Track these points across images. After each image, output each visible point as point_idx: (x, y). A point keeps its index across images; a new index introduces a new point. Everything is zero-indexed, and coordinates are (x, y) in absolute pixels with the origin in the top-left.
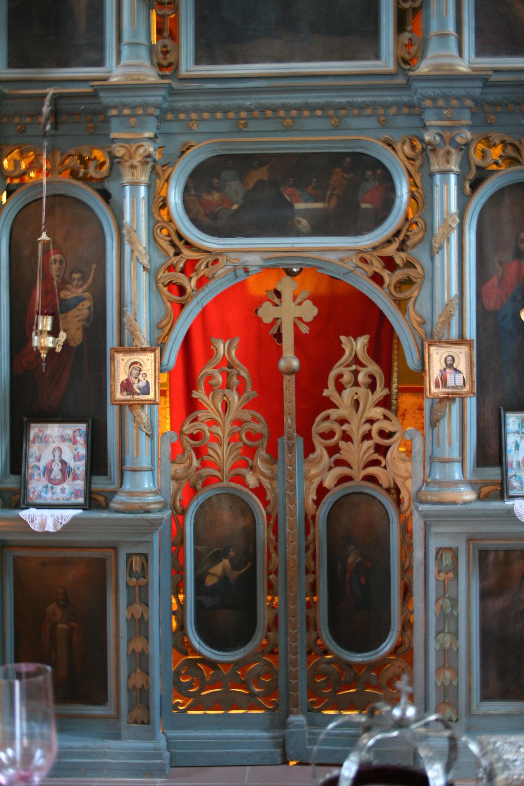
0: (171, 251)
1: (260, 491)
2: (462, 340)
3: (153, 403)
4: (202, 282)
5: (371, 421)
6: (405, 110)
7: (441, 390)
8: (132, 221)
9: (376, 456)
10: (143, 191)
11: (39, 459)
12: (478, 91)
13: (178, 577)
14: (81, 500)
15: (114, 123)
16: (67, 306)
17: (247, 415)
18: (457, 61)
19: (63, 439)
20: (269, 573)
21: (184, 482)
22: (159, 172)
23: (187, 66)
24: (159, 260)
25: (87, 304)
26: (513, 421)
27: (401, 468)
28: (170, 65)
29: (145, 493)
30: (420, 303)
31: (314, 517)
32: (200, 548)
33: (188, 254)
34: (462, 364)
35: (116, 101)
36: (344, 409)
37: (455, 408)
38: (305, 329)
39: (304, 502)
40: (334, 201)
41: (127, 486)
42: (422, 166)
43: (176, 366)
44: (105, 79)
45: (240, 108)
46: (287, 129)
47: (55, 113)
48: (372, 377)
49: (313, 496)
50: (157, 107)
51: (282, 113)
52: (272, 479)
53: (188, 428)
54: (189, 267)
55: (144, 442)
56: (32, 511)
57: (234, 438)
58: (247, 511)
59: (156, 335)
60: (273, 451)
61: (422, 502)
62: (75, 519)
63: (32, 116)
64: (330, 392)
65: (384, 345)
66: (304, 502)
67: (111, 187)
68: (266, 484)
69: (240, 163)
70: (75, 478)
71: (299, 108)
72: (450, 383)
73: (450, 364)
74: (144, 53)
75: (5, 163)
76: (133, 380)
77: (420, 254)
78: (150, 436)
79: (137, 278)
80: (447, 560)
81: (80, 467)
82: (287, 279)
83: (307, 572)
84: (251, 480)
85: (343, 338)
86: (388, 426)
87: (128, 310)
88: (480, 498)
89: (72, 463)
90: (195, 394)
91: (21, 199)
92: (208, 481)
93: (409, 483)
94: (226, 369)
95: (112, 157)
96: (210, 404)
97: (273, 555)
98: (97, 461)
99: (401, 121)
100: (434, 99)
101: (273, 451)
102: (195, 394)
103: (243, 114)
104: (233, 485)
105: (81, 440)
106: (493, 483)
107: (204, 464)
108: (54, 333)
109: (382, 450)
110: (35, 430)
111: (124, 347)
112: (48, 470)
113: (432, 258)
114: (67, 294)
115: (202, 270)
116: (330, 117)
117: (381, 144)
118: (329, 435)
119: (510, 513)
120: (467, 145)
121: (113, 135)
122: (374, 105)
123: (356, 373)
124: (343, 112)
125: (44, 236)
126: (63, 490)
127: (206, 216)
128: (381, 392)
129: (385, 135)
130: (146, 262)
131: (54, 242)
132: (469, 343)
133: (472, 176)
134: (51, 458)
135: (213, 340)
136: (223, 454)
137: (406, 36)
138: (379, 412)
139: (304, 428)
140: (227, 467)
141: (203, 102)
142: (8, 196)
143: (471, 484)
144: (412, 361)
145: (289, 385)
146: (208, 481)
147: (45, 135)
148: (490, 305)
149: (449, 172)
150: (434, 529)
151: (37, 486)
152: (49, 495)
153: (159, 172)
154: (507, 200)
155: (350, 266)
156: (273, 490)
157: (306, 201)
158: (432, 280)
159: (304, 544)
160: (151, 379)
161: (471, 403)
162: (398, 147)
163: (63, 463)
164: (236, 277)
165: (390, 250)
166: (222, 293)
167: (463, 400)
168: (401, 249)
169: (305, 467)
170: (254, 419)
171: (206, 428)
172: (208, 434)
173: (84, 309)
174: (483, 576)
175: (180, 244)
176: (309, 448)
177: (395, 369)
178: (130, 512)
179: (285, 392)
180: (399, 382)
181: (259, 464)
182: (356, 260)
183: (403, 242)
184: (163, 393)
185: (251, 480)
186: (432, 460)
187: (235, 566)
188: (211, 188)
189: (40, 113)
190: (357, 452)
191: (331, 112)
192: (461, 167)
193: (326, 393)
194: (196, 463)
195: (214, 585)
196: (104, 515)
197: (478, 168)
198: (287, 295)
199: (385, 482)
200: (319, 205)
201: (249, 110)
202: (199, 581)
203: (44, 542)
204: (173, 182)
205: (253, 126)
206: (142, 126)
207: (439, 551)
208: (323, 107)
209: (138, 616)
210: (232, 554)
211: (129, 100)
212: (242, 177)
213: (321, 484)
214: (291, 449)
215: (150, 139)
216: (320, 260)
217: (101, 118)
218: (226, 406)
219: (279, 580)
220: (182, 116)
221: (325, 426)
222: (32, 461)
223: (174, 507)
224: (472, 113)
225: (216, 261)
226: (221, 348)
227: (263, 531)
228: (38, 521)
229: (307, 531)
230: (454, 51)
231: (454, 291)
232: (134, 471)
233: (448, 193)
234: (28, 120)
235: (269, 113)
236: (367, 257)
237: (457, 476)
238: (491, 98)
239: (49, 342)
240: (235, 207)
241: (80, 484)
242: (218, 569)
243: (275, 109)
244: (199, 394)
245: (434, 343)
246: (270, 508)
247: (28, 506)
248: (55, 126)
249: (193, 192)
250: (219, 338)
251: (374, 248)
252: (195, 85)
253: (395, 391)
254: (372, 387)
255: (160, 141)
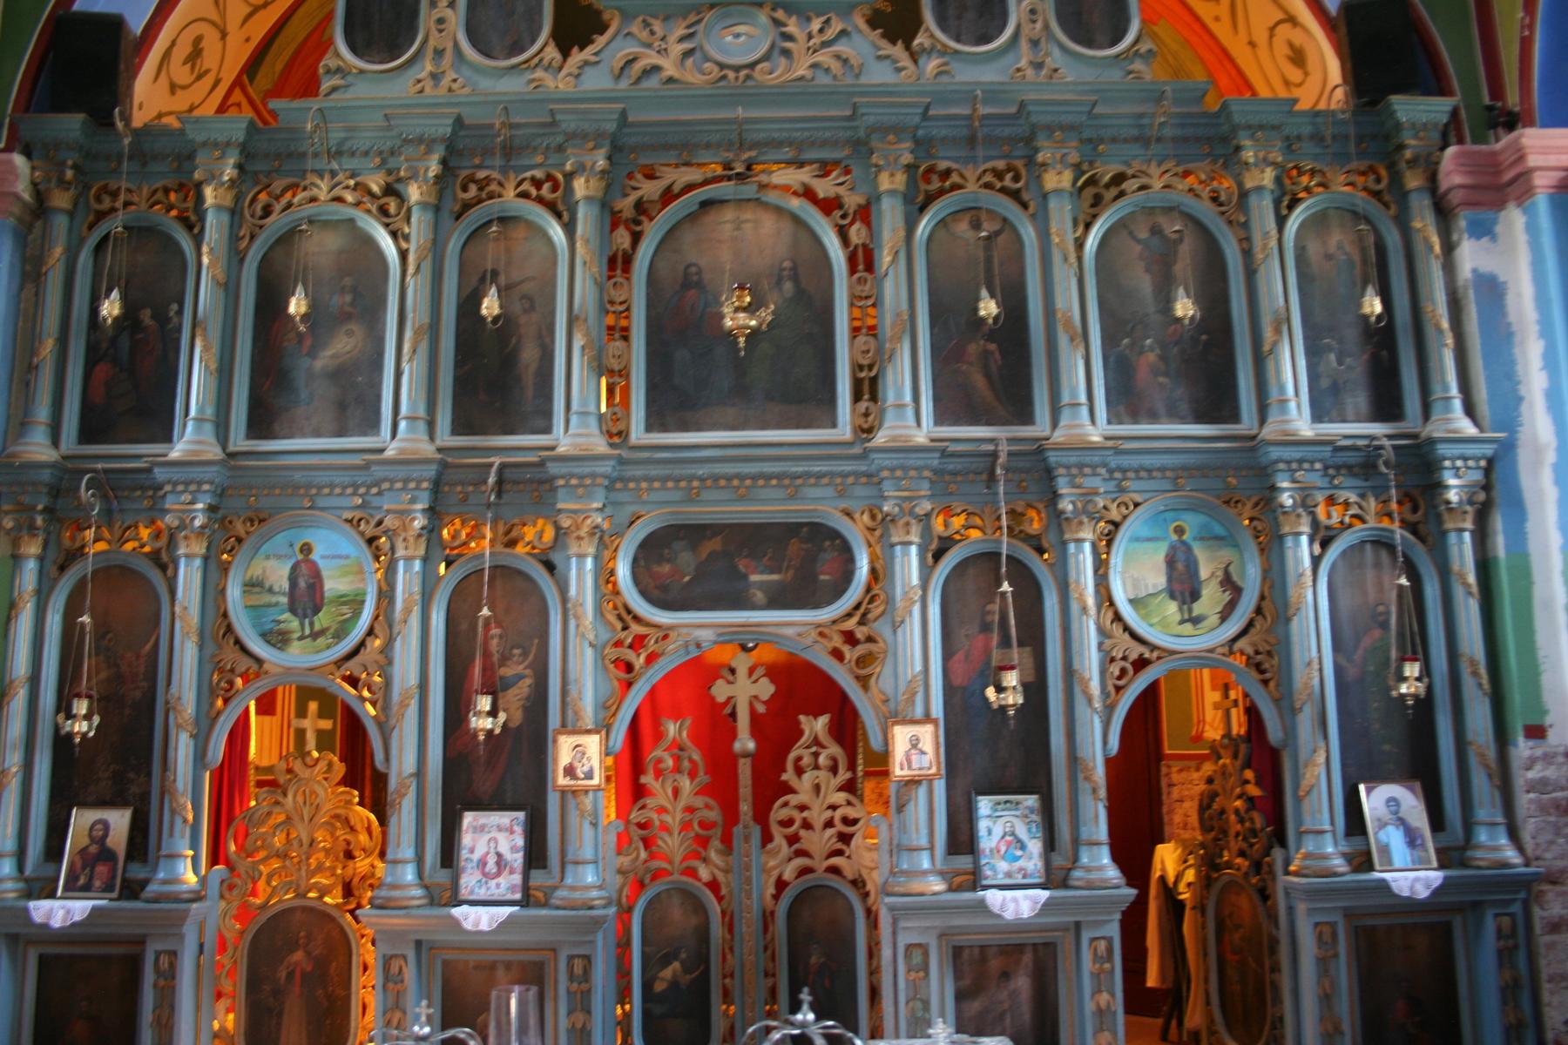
0: (619, 626)
1: (714, 885)
2: (927, 719)
3: (597, 789)
4: (651, 659)
5: (833, 807)
6: (864, 480)
7: (906, 772)
8: (578, 593)
9: (839, 846)
10: (589, 563)
11: (472, 851)
12: (936, 462)
13: (624, 982)
14: (518, 896)
15: (561, 493)
16: (507, 684)
17: (699, 802)
18: (914, 432)
19: (500, 829)
20: (724, 977)
21: (631, 876)
22: (605, 542)
23: (638, 432)
24: (605, 635)
25: (528, 681)
26: (984, 804)
27: (867, 856)
28: (619, 434)
29: (588, 888)
30: (884, 680)
31: (772, 913)
32: (647, 949)
33: (637, 629)
34: (927, 744)
35: (564, 471)
36: (803, 797)
37: (922, 792)
38: (761, 709)
39: (761, 897)
40: (791, 573)
41: (569, 881)
42: (882, 536)
43: (623, 750)
44: (553, 448)
45: (692, 478)
46: (742, 499)
47: (500, 482)
48: (834, 760)
49: (771, 890)
50: (606, 477)
51: (736, 482)
52: (726, 871)
53: (635, 816)
54: (638, 643)
55: (588, 832)
56: (465, 908)
57: (686, 826)
58: (699, 908)
59: (601, 716)
60: (727, 840)
61: (888, 895)
62: (511, 916)
63: (475, 485)
64: (788, 776)
65: (846, 727)
66: (761, 897)
67: (556, 558)
68: (721, 877)
69: (693, 533)
70: (512, 872)
71: (754, 478)
72: (915, 766)
73: (915, 743)
74: (593, 422)
75: (445, 532)
76: (576, 764)
77: (882, 628)
78: (594, 825)
79: (582, 654)
80: (917, 958)
81: (517, 859)
82: (742, 656)
83: (766, 975)
84: (704, 873)
85: (802, 718)
86: (852, 813)
87: (573, 689)
88: (951, 889)
89: (508, 856)
90: (644, 780)
91: (459, 571)
92: (657, 875)
93: (875, 874)
94: (676, 751)
95: (558, 528)
96: (659, 790)
97: (729, 956)
98: (535, 855)
99: (860, 491)
100: (892, 470)
101: (727, 840)
102: (644, 780)
103: (695, 484)
104: (685, 878)
105: (519, 829)
106: (966, 873)
107: (652, 856)
108: (493, 713)
109: (845, 838)
110: (469, 818)
111: (567, 728)
112: (482, 863)
113: (895, 632)
114: (507, 672)
115: (651, 646)
116: (787, 487)
117: (839, 515)
118: (788, 823)
119: (982, 906)
120: (928, 515)
121: (560, 506)
122: (832, 475)
123: (816, 755)
124: (799, 481)
125: (485, 611)
126: (498, 886)
127: (657, 587)
128: (843, 775)
129: (843, 505)
130: (591, 637)
131: (495, 616)
132: (935, 722)
133: (934, 546)
134: (485, 850)
135: (664, 720)
136: (673, 844)
137: (863, 405)
138: (841, 797)
139: (761, 816)
140: (678, 858)
141: (654, 471)
142: (447, 567)
143: (941, 873)
144: (876, 743)
145: (745, 769)
146: (657, 875)
147: (489, 505)
148: (957, 681)
149: (910, 543)
150: (902, 924)
151: (470, 882)
152: (483, 891)
153: (605, 542)
154: (971, 571)
155: (809, 641)
156: (728, 885)
157: (762, 573)
158: (895, 654)
159: (762, 944)
160: (596, 763)
161: (940, 787)
162: (857, 516)
163: (499, 855)
164: (688, 653)
165: (851, 624)
166: (674, 671)
167: (931, 781)
168: (861, 623)
169: (763, 858)
170: (707, 807)
171: (655, 816)
172: (657, 823)
173: (524, 688)
174: (958, 975)
175: (628, 618)
176: (767, 838)
177: (860, 750)
178: (573, 909)
179: (741, 777)
180: (865, 764)
181: (713, 855)
182: (814, 634)
183: (864, 615)
184: (608, 779)
185: (704, 873)
186: (899, 848)
187: (686, 970)
188: (661, 560)
189: (485, 482)
190: (819, 841)
191: (787, 482)
192: (922, 537)
193: (784, 777)
194: (643, 855)
195: (664, 991)
196: (544, 912)
197: (940, 538)
198: (742, 671)
199: (849, 873)
200: (775, 577)
201: (702, 479)
202: (647, 986)
203: (478, 943)
204: (621, 554)
205: (705, 495)
206: (589, 496)
207: (909, 947)
208: (779, 477)
209: (579, 1026)
210: (683, 956)
211: (577, 470)
212: (694, 547)
213: (780, 877)
214: (747, 839)
215: (597, 509)
216: (777, 635)
217: (547, 486)
218: (676, 792)
219: (735, 985)
220: (632, 485)
221: (784, 814)
222: (464, 854)
223: (619, 903)
224: (932, 482)
225: (665, 637)
226: (672, 729)
227: (717, 930)
228: (471, 919)
229: (766, 929)
230: (911, 421)
231: (918, 667)
232: (577, 863)
233: (909, 565)
234: (471, 488)
235: (723, 483)
236: (826, 631)
237: (926, 864)
238: (951, 467)
239: (488, 723)
240: (687, 579)
241: (517, 878)
242: (667, 973)
243: (729, 478)
244: (647, 779)
245: (897, 723)
246: (724, 903)
247: (460, 903)
248: (499, 495)
249: (642, 563)
250: (669, 717)
251: (834, 622)
252: (646, 455)
253: (860, 774)
254: (834, 770)
255: (608, 511)
